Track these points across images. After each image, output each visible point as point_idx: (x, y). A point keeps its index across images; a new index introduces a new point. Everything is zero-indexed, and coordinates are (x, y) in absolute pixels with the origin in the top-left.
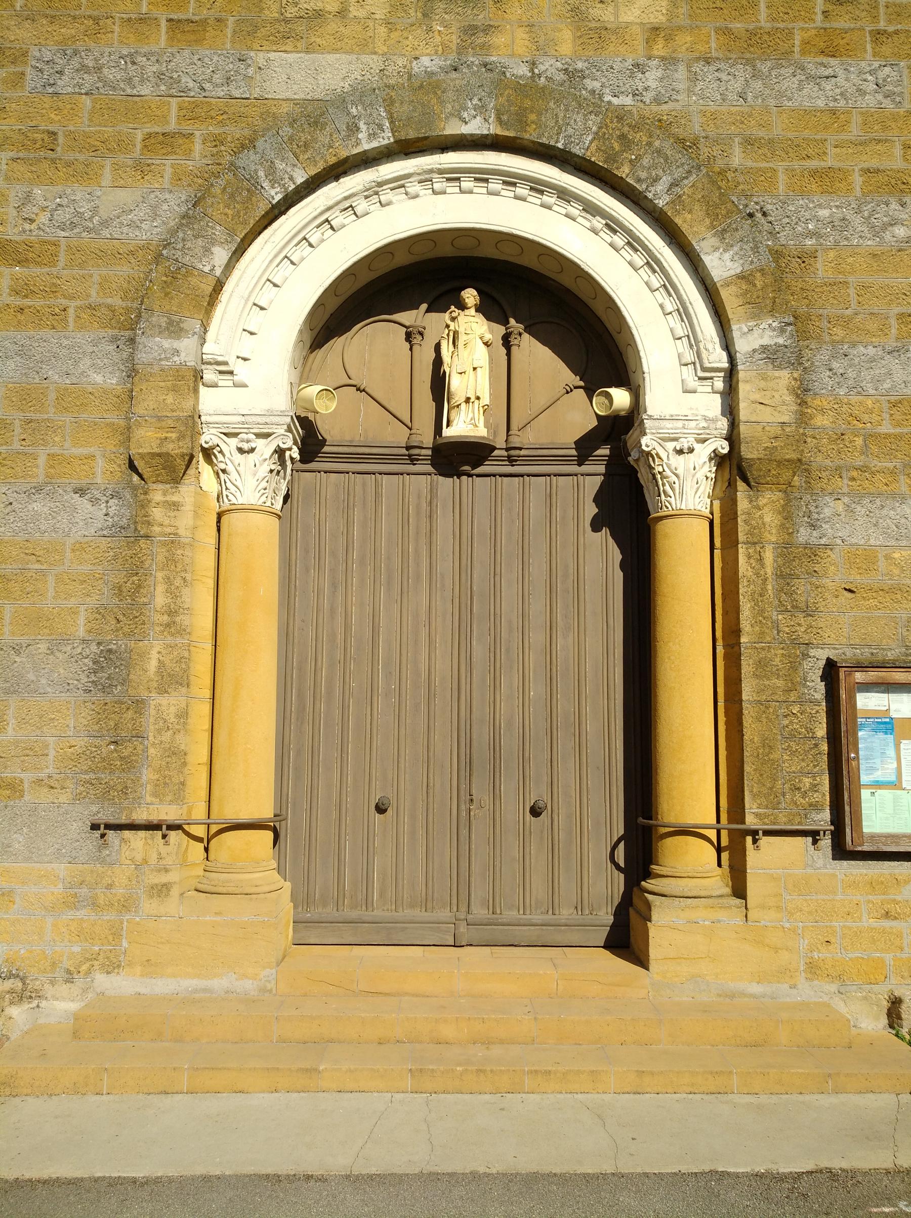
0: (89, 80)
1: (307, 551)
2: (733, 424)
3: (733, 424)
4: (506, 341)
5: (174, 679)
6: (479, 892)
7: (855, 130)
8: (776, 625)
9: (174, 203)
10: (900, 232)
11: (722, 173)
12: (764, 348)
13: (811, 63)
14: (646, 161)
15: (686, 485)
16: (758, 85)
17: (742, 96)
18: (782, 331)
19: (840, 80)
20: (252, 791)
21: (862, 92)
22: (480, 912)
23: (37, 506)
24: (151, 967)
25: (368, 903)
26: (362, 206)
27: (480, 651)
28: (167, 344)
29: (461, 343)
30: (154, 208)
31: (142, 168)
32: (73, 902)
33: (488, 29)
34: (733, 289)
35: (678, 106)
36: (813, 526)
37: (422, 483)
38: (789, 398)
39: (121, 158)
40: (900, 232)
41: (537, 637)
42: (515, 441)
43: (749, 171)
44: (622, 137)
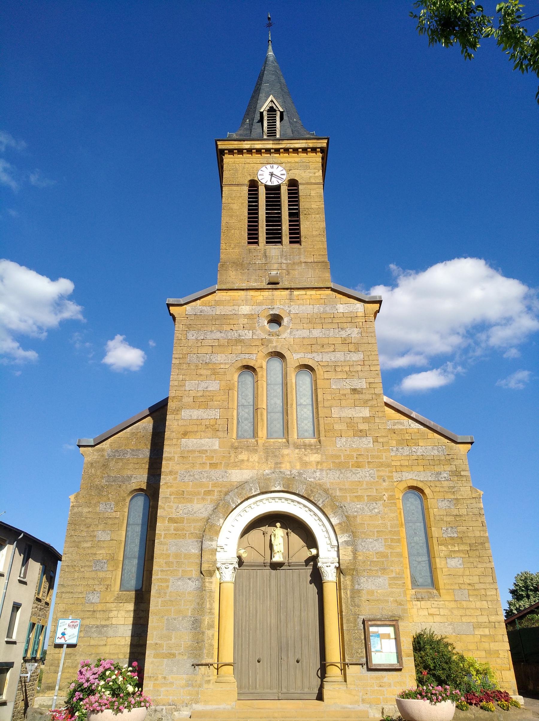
0: (192, 478)
1: (239, 591)
2: (339, 559)
3: (339, 559)
4: (287, 533)
5: (210, 626)
6: (284, 684)
7: (365, 486)
8: (351, 610)
9: (210, 507)
10: (376, 510)
11: (335, 497)
12: (345, 541)
13: (354, 469)
14: (316, 496)
15: (330, 575)
16: (342, 475)
17: (338, 478)
18: (349, 537)
19: (361, 474)
20: (228, 656)
21: (366, 477)
22: (284, 690)
23: (179, 583)
24: (206, 702)
25: (256, 688)
26: (253, 506)
27: (283, 617)
28: (210, 543)
29: (276, 537)
30: (206, 509)
31: (203, 499)
32: (188, 685)
33: (280, 463)
34: (337, 527)
35: (324, 481)
36: (359, 585)
37: (268, 571)
38: (351, 553)
39: (199, 497)
40: (376, 510)
41: (297, 613)
42: (290, 561)
43: (340, 496)
44: (311, 490)
